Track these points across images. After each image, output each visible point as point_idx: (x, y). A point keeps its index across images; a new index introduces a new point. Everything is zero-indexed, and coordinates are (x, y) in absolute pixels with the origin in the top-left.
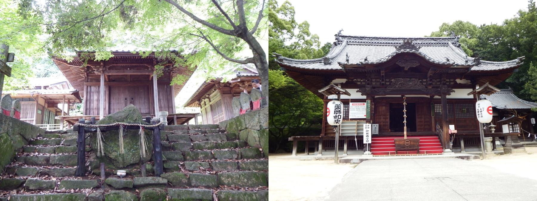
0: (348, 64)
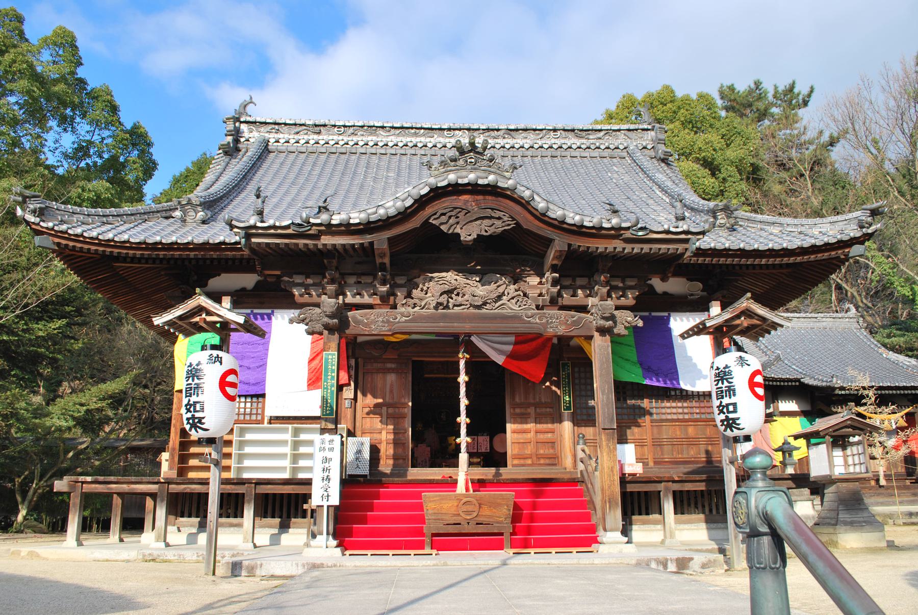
0: (259, 224)
